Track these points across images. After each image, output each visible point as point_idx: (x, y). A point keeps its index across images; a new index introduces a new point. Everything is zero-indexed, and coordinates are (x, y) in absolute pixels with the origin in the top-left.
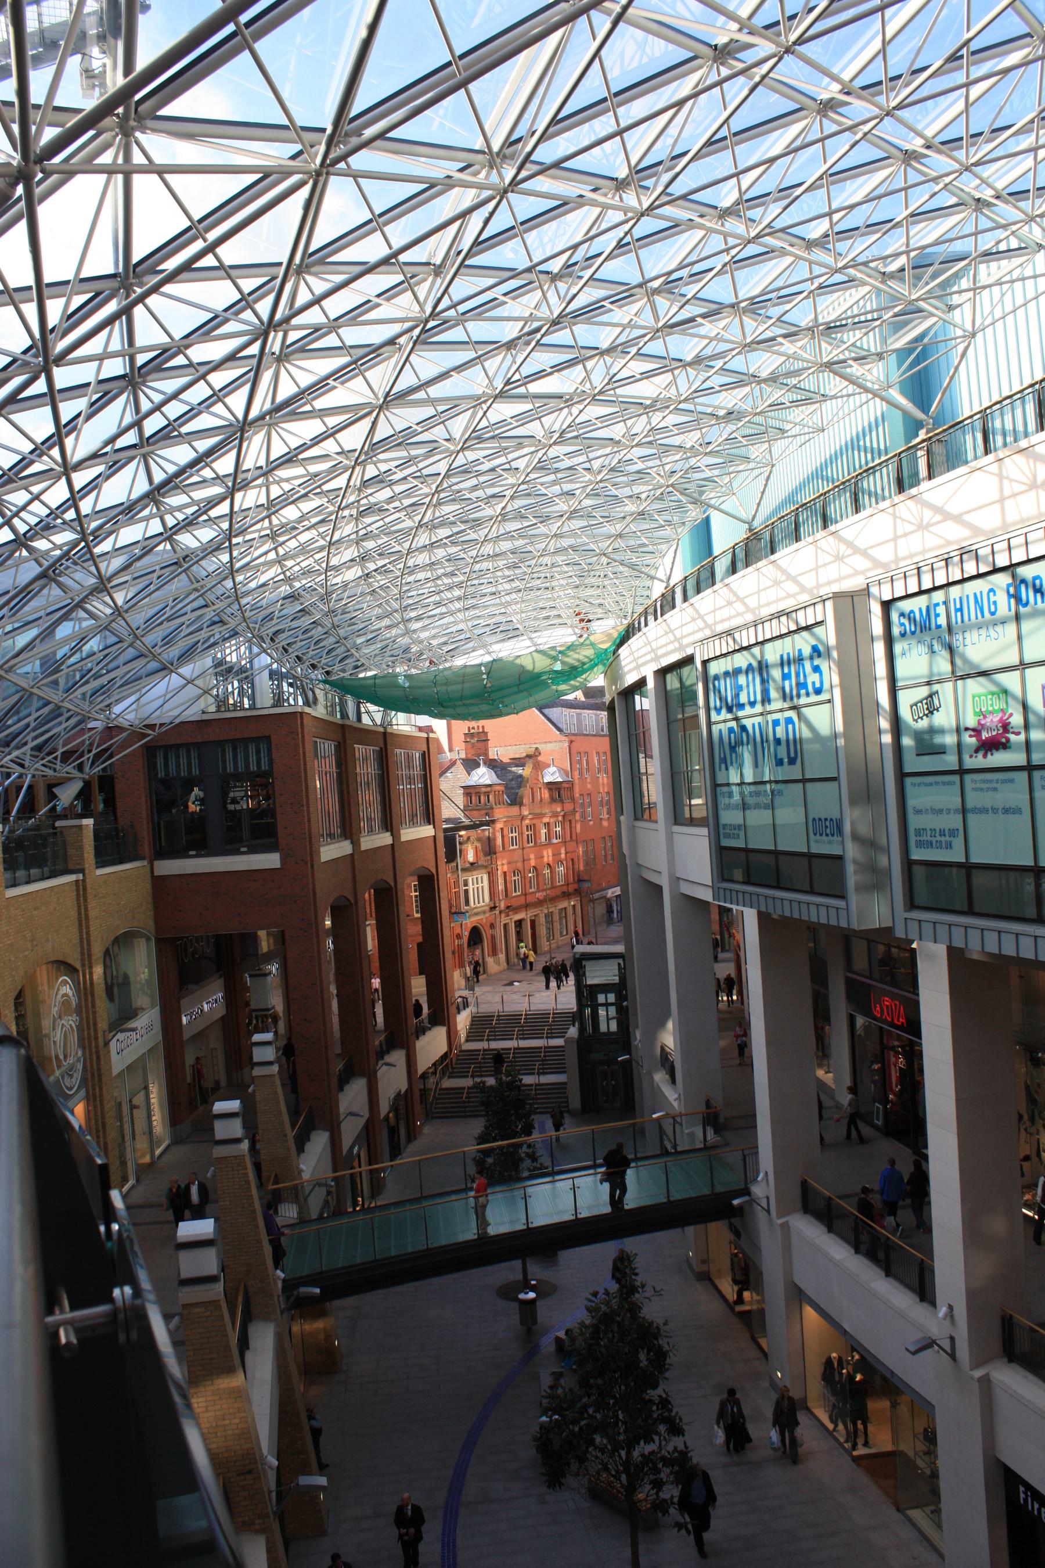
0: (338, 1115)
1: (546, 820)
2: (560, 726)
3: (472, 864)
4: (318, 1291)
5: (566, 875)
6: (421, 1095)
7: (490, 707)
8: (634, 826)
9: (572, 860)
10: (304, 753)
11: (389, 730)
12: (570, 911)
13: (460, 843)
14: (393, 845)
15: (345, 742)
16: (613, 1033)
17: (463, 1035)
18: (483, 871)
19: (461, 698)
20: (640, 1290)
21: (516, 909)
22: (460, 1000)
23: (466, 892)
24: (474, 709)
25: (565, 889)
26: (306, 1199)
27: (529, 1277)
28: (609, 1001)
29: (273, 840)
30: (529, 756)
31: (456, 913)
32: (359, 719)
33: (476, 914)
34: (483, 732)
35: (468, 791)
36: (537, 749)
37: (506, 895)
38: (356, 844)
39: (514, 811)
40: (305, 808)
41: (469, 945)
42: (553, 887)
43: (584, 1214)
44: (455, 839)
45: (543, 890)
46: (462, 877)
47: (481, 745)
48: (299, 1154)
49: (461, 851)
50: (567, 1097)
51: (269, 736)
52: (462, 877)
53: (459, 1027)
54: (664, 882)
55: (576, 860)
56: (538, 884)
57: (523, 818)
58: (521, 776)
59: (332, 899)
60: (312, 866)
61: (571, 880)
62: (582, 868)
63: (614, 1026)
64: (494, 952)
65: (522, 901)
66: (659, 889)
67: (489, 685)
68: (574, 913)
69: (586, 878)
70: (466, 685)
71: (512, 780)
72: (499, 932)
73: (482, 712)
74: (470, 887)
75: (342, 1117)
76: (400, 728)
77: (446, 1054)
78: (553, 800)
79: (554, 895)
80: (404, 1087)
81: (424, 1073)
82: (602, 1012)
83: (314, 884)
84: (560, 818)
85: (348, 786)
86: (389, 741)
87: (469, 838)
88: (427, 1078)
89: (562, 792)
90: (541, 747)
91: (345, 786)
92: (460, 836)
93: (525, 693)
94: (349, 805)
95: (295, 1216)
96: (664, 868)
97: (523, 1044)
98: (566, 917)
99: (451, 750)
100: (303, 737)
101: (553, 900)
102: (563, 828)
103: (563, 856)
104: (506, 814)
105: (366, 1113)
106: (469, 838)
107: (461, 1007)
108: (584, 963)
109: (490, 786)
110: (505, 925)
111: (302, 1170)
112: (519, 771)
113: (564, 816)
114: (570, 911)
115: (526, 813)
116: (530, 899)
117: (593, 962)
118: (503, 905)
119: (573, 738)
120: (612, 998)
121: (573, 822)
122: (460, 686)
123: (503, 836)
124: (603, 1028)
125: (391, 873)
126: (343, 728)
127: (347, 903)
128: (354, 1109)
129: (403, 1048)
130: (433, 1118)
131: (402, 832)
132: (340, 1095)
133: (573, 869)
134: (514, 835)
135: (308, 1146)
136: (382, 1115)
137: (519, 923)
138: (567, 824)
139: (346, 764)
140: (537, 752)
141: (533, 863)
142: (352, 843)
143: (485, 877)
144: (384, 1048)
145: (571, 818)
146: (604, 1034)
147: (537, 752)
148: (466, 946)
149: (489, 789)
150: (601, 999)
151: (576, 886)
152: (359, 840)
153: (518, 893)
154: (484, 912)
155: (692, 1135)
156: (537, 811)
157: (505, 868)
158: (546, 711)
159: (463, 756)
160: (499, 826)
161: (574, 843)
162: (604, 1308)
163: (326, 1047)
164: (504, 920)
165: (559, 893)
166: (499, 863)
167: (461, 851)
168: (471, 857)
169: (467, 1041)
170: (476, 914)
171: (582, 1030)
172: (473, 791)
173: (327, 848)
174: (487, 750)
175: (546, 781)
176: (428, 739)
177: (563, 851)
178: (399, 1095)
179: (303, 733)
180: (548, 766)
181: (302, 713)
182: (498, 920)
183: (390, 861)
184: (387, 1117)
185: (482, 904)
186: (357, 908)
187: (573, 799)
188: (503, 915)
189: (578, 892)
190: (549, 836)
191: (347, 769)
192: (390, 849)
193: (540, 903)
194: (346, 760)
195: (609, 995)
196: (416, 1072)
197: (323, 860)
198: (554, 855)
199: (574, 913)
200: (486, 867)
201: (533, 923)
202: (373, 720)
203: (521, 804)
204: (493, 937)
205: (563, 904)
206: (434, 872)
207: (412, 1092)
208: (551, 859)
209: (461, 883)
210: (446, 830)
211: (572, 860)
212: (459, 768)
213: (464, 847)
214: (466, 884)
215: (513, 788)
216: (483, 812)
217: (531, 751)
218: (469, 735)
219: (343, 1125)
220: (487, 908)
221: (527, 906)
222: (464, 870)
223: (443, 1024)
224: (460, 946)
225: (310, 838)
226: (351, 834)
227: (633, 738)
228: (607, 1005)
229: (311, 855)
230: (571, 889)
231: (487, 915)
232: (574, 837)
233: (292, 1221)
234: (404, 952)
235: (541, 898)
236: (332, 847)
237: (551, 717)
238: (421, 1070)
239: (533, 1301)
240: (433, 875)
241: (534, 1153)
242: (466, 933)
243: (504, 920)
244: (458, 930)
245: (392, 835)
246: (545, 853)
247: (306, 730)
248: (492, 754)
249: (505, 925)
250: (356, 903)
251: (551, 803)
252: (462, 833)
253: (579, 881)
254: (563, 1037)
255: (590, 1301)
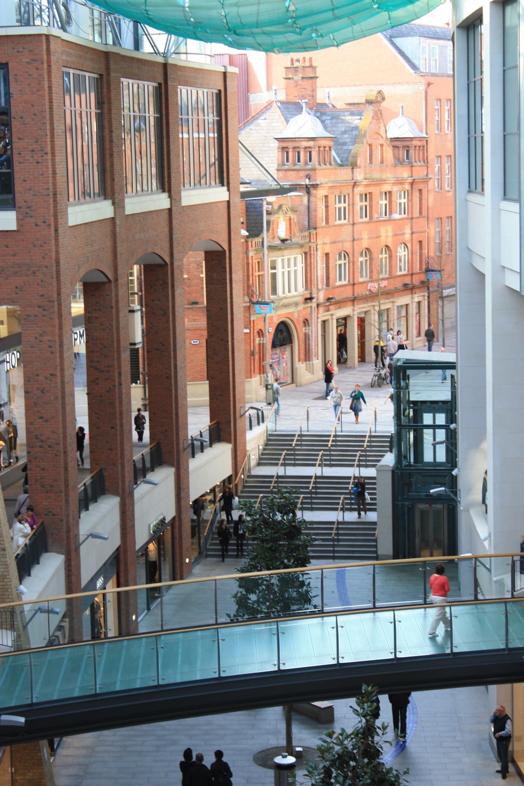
0: (77, 536)
1: (386, 188)
2: (416, 62)
3: (283, 241)
4: (22, 720)
5: (411, 262)
6: (193, 528)
7: (298, 37)
8: (466, 200)
9: (420, 242)
10: (50, 88)
11: (170, 61)
12: (413, 309)
13: (269, 213)
14: (170, 210)
15: (108, 74)
16: (441, 464)
17: (254, 458)
18: (299, 251)
19: (257, 25)
20: (380, 732)
21: (340, 303)
22: (253, 412)
23: (274, 276)
24: (279, 39)
25: (407, 280)
26: (25, 627)
27: (294, 743)
28: (438, 423)
29: (10, 196)
30: (369, 102)
31: (258, 303)
32: (137, 45)
33: (286, 306)
34: (311, 66)
35: (285, 145)
36: (379, 92)
37: (328, 285)
38: (118, 205)
39: (344, 174)
40: (49, 157)
41: (274, 346)
42: (391, 277)
43: (347, 658)
44: (261, 206)
45: (377, 281)
46: (268, 257)
47: (306, 84)
48: (21, 580)
49: (268, 223)
50: (376, 541)
51: (7, 64)
52: (268, 257)
53: (248, 447)
54: (487, 269)
55: (425, 244)
56: (371, 272)
57: (355, 185)
58: (356, 128)
59: (82, 272)
60: (56, 230)
61: (417, 269)
62: (432, 254)
63: (441, 457)
64: (307, 357)
65: (348, 293)
66: (482, 276)
67: (292, 8)
68: (419, 312)
69: (436, 267)
70: (263, 7)
71: (345, 132)
72: (316, 330)
73: (290, 43)
74: (279, 271)
75: (82, 538)
76: (190, 58)
77: (230, 478)
78: (399, 162)
79: (392, 287)
80: (170, 514)
81: (196, 502)
82: (428, 434)
83: (57, 252)
84: (407, 187)
85: (111, 132)
86: (170, 76)
87: (280, 207)
88: (203, 508)
89: (412, 152)
90: (386, 90)
91: (107, 131)
92: (268, 203)
93: (345, 21)
94: (111, 155)
95: (10, 644)
96: (487, 254)
97: (329, 471)
98: (407, 316)
99: (269, 88)
100: (49, 66)
101: (388, 294)
102: (410, 200)
103: (407, 236)
104: (333, 177)
105: (115, 542)
106: (280, 207)
107: (254, 421)
108: (409, 372)
109: (313, 139)
110: (324, 322)
111: (22, 593)
112: (355, 121)
113: (412, 184)
114: (413, 309)
115: (359, 176)
116: (359, 291)
117: (422, 373)
118: (321, 297)
119: (431, 79)
120: (441, 419)
121: (424, 192)
122: (254, 9)
123: (327, 207)
124: (428, 457)
125: (167, 245)
126: (107, 55)
127: (105, 280)
128: (99, 531)
129: (171, 465)
130: (207, 556)
131: (183, 194)
132: (83, 514)
133: (421, 255)
134: (342, 205)
135: (36, 571)
136: (138, 545)
137: (344, 321)
138: (416, 194)
139: (110, 103)
140: (381, 97)
141: (365, 244)
142: (114, 204)
143: (300, 259)
144: (148, 465)
145: (421, 186)
146: (429, 464)
147: (381, 97)
148: (269, 345)
149: (311, 144)
150: (427, 419)
151: (423, 277)
152: (123, 201)
153: (344, 282)
154: (296, 304)
155: (500, 583)
156: (376, 175)
157: (328, 249)
158: (398, 41)
159: (282, 97)
160: (321, 193)
161: (424, 220)
162: (337, 748)
163: (65, 452)
164: (323, 315)
165: (398, 284)
166: (319, 242)
167: (268, 223)
168: (282, 232)
169: (259, 464)
170: (286, 306)
171: (400, 458)
172: (290, 145)
173: (78, 208)
174: (314, 90)
175: (390, 136)
176: (225, 74)
177: (408, 231)
178: (163, 521)
179: (49, 61)
180: (396, 115)
181: (47, 36)
182: (314, 315)
183: (166, 230)
184: (145, 548)
185: (293, 293)
186: (117, 286)
187: (426, 161)
188: (321, 309)
189: (425, 285)
190: (389, 209)
191: (110, 110)
192: (166, 215)
193: (372, 296)
194: (109, 99)
195: (438, 415)
196: (188, 496)
197: (70, 224)
198: (395, 235)
199: (419, 312)
200: (301, 246)
201: (362, 322)
202: (154, 46)
203: (354, 166)
204: (307, 337)
205: (404, 300)
206: (226, 248)
207: (180, 520)
208: (390, 239)
209: (267, 264)
210: (244, 195)
211: (420, 242)
212: (276, 113)
213: (272, 218)
214: (274, 268)
215: (345, 144)
216: (303, 174)
217: (372, 97)
218: (292, 69)
219: (82, 548)
220: (301, 299)
221: (354, 300)
222: (272, 248)
223: (228, 441)
224: (262, 346)
225: (55, 194)
226: (113, 193)
227: (472, 86)
228: (434, 427)
229: (56, 216)
230: (416, 280)
231: (301, 307)
232: (425, 213)
233: (8, 650)
234: (178, 345)
235: (374, 290)
236: (85, 207)
237: (404, 49)
238: (194, 495)
239: (291, 767)
240: (224, 251)
241: (307, 592)
242: (272, 330)
243: (323, 315)
244: (259, 326)
245: (170, 197)
246: (383, 234)
247: (53, 58)
248: (321, 97)
249: (324, 322)
250: (116, 280)
251: (395, 165)
252: (271, 199)
253: (428, 270)
254: (374, 466)
255: (325, 741)
